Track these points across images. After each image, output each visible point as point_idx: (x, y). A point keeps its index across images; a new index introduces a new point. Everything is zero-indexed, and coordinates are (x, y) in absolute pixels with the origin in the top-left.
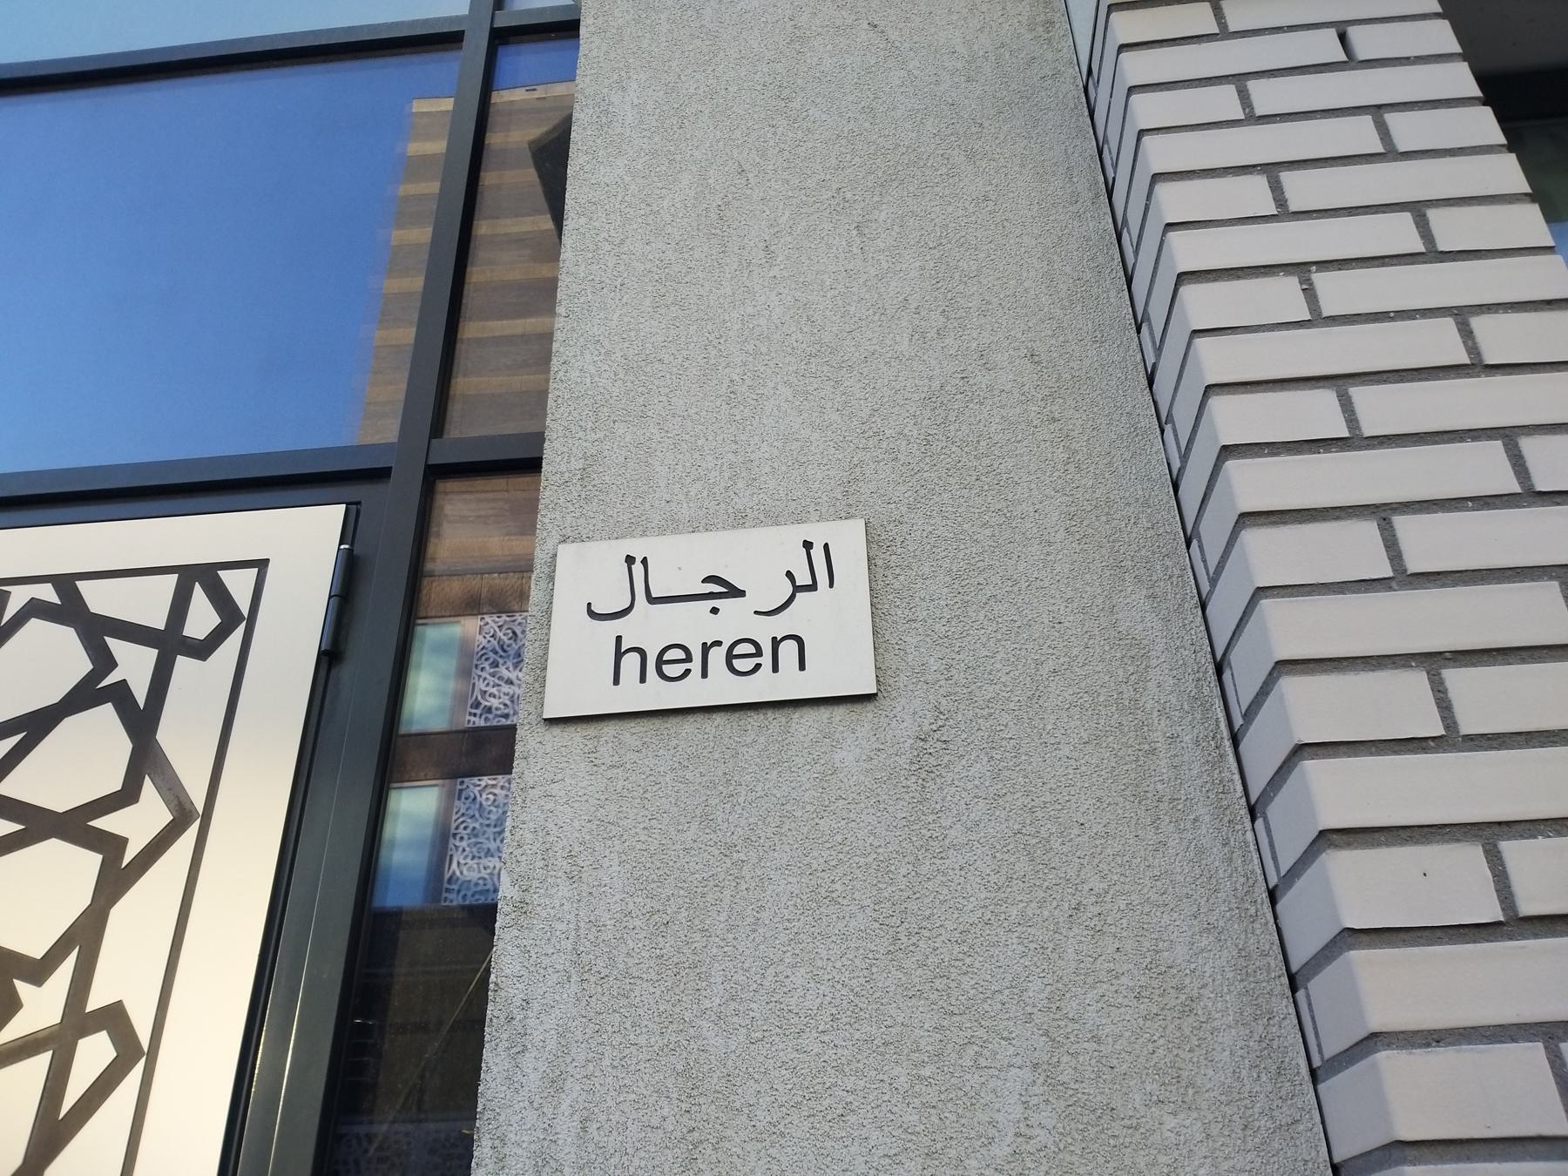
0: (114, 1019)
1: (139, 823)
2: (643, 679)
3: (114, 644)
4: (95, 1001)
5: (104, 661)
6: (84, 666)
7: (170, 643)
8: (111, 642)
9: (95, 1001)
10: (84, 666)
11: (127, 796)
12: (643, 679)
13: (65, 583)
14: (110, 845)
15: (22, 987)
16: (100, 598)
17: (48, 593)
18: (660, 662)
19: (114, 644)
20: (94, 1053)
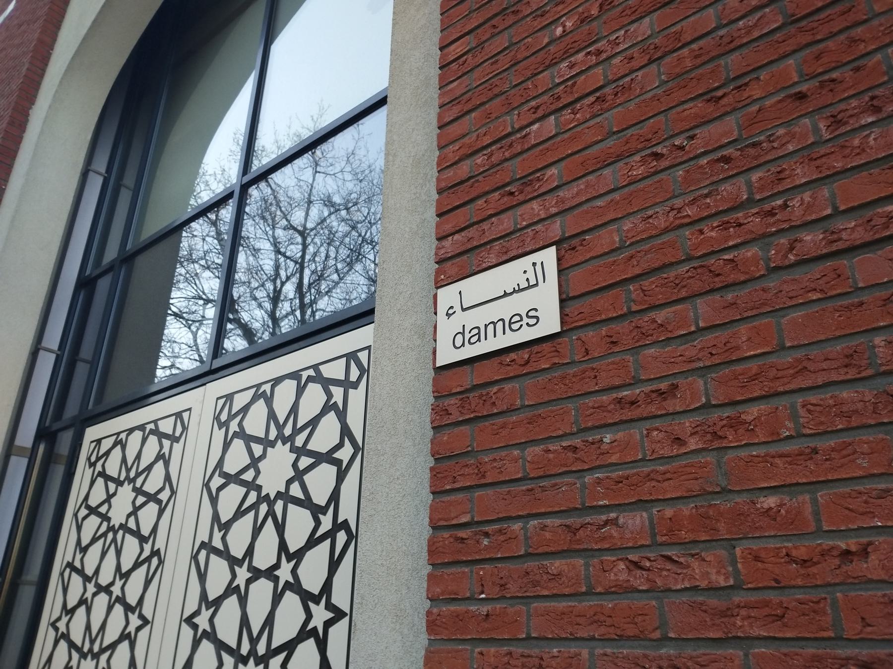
0: (345, 525)
1: (345, 454)
2: (504, 333)
3: (336, 455)
4: (340, 520)
5: (329, 395)
6: (334, 469)
7: (347, 385)
8: (339, 522)
9: (340, 520)
10: (334, 469)
11: (340, 446)
12: (504, 333)
13: (315, 367)
14: (337, 463)
15: (277, 573)
16: (328, 371)
17: (311, 372)
18: (510, 323)
19: (336, 455)
20: (342, 537)
